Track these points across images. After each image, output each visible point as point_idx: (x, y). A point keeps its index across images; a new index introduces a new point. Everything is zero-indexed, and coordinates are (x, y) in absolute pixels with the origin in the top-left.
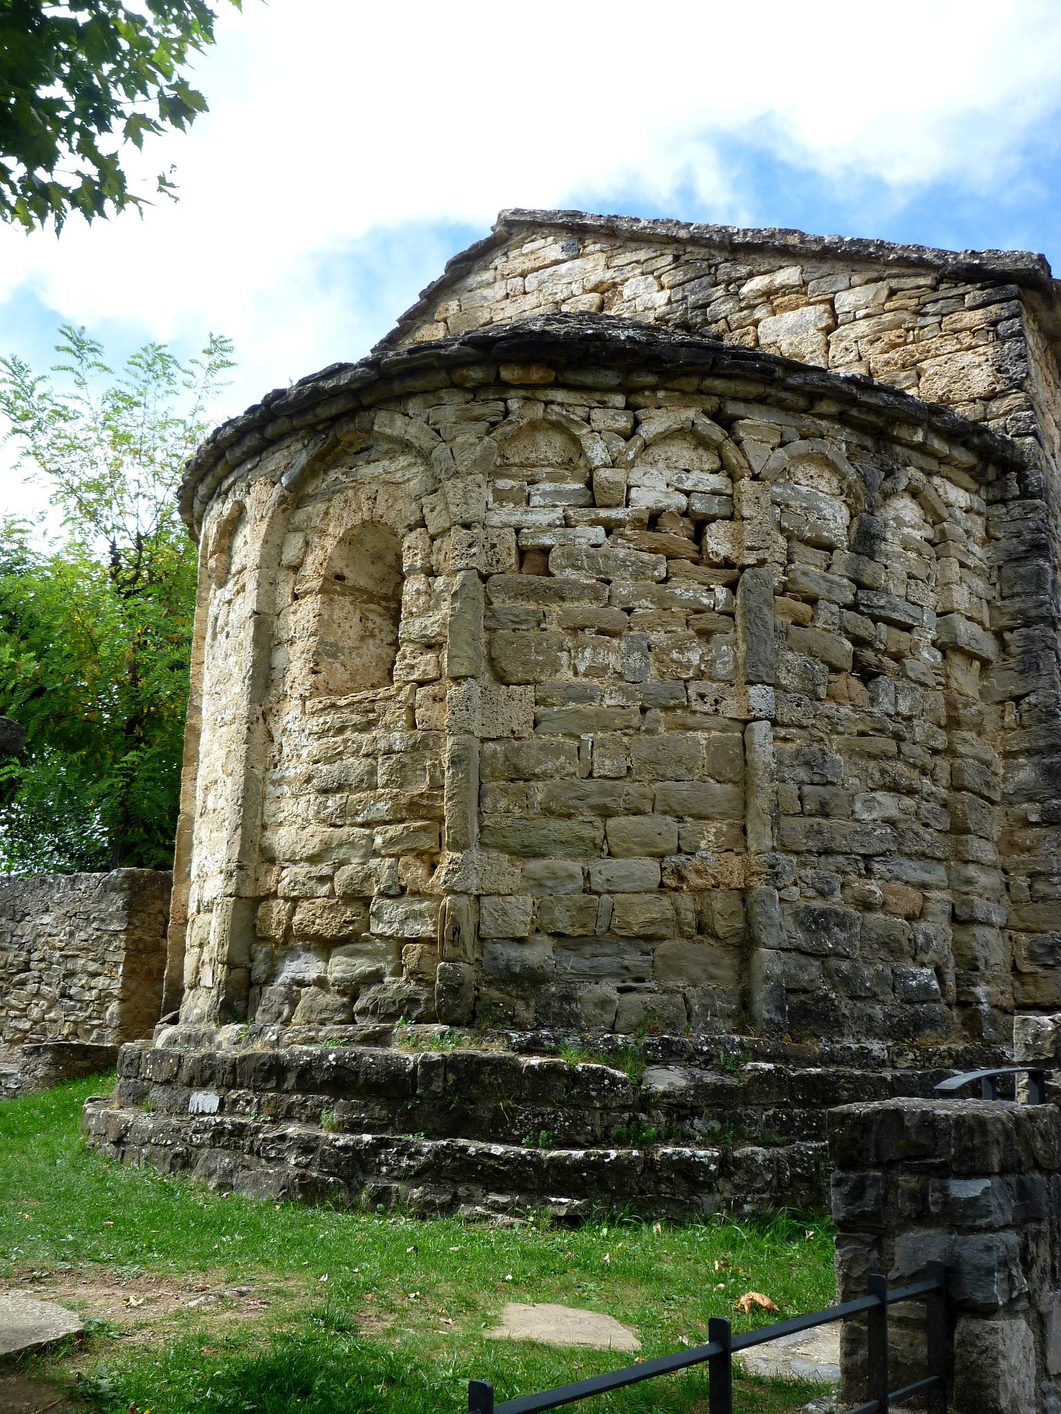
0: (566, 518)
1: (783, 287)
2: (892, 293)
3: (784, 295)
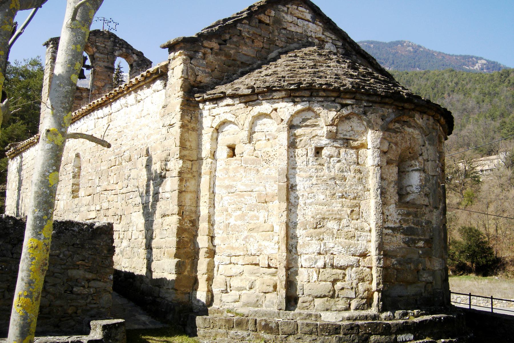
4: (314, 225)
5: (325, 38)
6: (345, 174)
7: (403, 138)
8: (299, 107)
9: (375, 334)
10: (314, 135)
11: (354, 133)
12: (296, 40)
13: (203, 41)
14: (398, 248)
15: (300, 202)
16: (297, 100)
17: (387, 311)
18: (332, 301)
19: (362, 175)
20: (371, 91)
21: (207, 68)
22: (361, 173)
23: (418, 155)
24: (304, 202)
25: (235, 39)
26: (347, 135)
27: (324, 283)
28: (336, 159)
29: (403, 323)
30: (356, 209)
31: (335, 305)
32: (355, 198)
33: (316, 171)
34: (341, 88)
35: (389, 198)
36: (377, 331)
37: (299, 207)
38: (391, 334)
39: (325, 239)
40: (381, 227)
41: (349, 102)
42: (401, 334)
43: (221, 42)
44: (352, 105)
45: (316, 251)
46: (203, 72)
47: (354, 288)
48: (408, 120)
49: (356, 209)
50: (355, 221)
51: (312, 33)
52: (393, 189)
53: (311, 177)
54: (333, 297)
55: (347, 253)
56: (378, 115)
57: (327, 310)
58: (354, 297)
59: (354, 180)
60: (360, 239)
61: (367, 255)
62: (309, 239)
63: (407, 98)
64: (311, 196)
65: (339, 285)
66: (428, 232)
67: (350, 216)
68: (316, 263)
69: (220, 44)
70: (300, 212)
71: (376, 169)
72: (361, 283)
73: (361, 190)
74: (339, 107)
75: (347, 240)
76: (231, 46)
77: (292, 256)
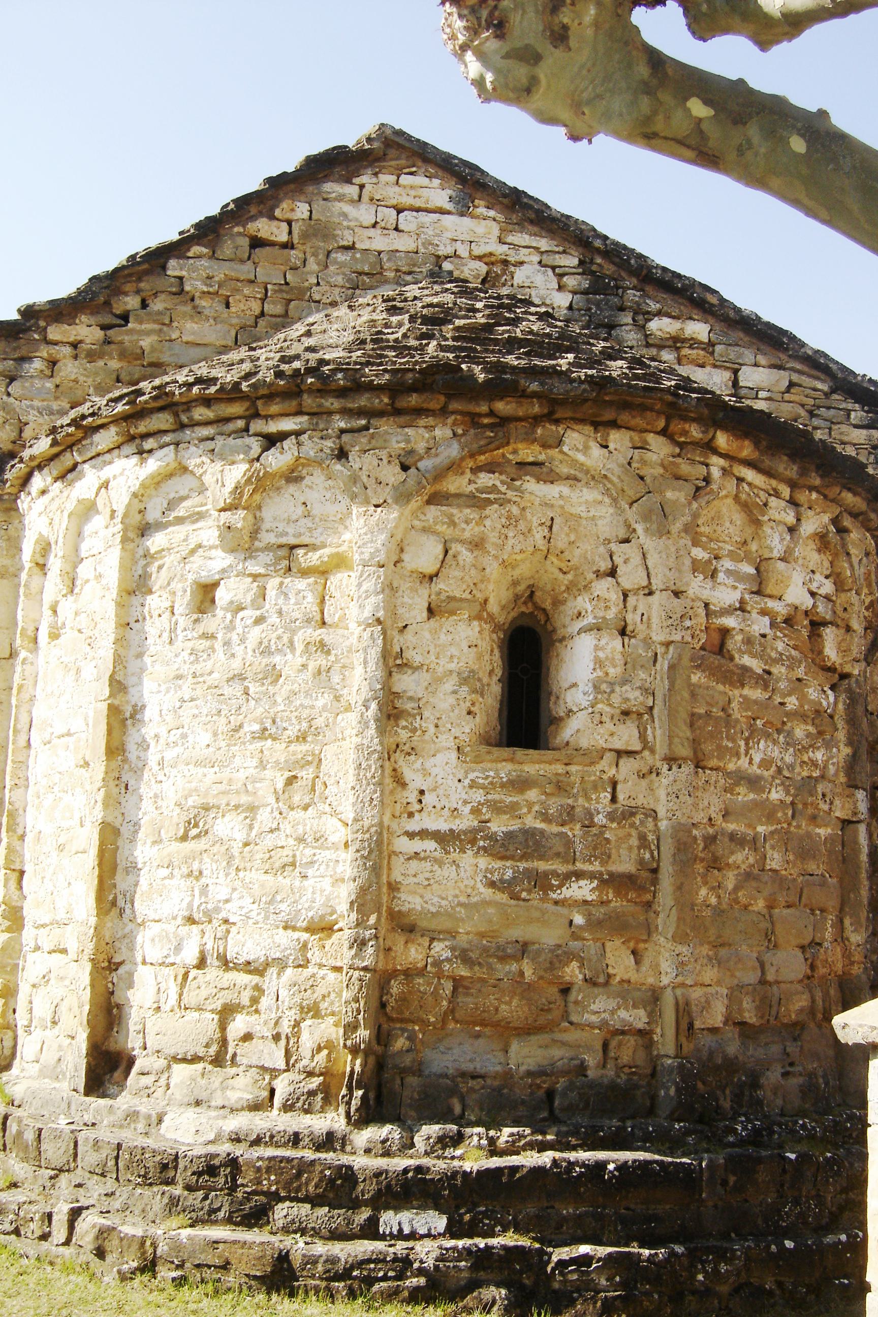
0: (742, 601)
1: (692, 339)
2: (792, 385)
3: (691, 347)
4: (178, 829)
5: (512, 252)
6: (277, 659)
7: (511, 521)
8: (153, 465)
9: (292, 1200)
10: (192, 546)
11: (310, 525)
12: (391, 275)
13: (46, 328)
14: (460, 904)
15: (150, 757)
16: (149, 444)
17: (382, 1120)
18: (218, 1075)
19: (332, 658)
20: (340, 376)
21: (56, 398)
22: (328, 653)
23: (592, 576)
24: (159, 756)
25: (157, 305)
26: (287, 534)
27: (196, 1015)
28: (250, 614)
29: (406, 1171)
30: (307, 774)
31: (224, 1089)
32: (302, 738)
33: (193, 658)
34: (244, 386)
35: (432, 730)
36: (298, 1190)
37: (146, 775)
38: (355, 1205)
39: (205, 873)
40: (373, 830)
41: (287, 425)
42: (397, 1209)
43: (108, 319)
44: (298, 434)
45: (181, 913)
46: (41, 413)
47: (283, 1037)
48: (542, 457)
49: (307, 774)
50: (298, 814)
51: (459, 243)
52: (451, 700)
53: (179, 677)
54: (218, 1061)
55: (267, 918)
56: (383, 454)
57: (198, 1103)
58: (283, 1066)
59: (303, 676)
60: (310, 873)
61: (336, 927)
62: (165, 872)
63: (487, 382)
64: (174, 739)
65: (239, 1025)
66: (630, 848)
67: (281, 797)
68: (178, 948)
69: (104, 327)
70: (147, 788)
71: (366, 635)
72: (308, 1022)
73: (324, 708)
74: (256, 445)
75: (269, 877)
76: (143, 327)
77: (125, 925)
